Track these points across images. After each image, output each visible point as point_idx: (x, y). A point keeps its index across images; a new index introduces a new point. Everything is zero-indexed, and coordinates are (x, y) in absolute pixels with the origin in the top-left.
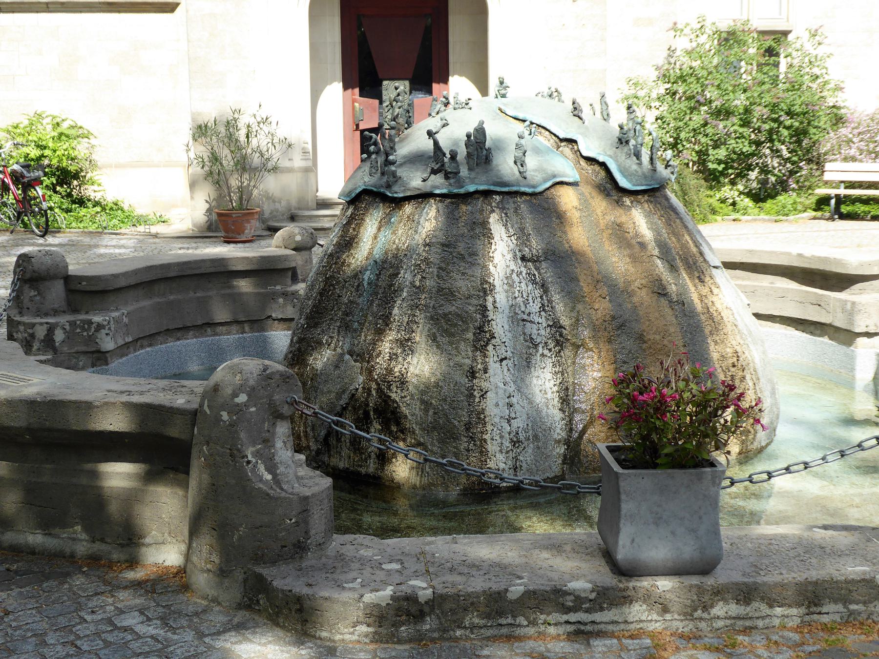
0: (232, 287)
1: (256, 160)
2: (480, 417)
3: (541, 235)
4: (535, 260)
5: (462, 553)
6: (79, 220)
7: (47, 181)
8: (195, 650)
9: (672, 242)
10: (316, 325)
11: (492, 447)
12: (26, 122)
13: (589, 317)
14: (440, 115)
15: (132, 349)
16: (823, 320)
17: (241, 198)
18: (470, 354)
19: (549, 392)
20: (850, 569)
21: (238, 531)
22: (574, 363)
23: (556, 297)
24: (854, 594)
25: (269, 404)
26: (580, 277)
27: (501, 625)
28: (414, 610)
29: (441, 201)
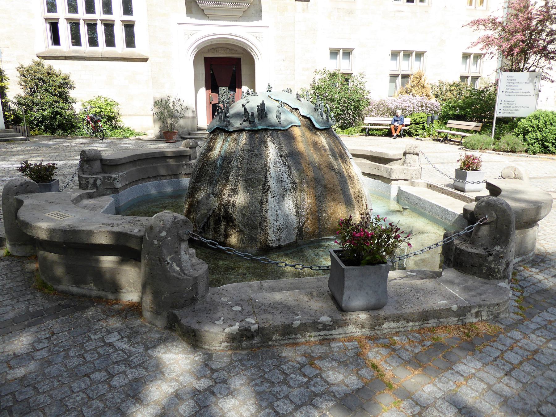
0: (167, 162)
1: (176, 114)
2: (265, 220)
3: (287, 147)
4: (285, 157)
5: (268, 300)
6: (115, 134)
7: (103, 120)
8: (143, 359)
9: (335, 149)
10: (198, 182)
11: (270, 232)
12: (95, 100)
13: (306, 179)
14: (246, 98)
15: (128, 186)
16: (379, 175)
17: (171, 127)
18: (261, 195)
19: (291, 209)
20: (439, 302)
21: (164, 295)
22: (300, 197)
23: (294, 172)
24: (442, 315)
25: (177, 235)
26: (302, 163)
27: (289, 339)
28: (249, 334)
29: (247, 133)
